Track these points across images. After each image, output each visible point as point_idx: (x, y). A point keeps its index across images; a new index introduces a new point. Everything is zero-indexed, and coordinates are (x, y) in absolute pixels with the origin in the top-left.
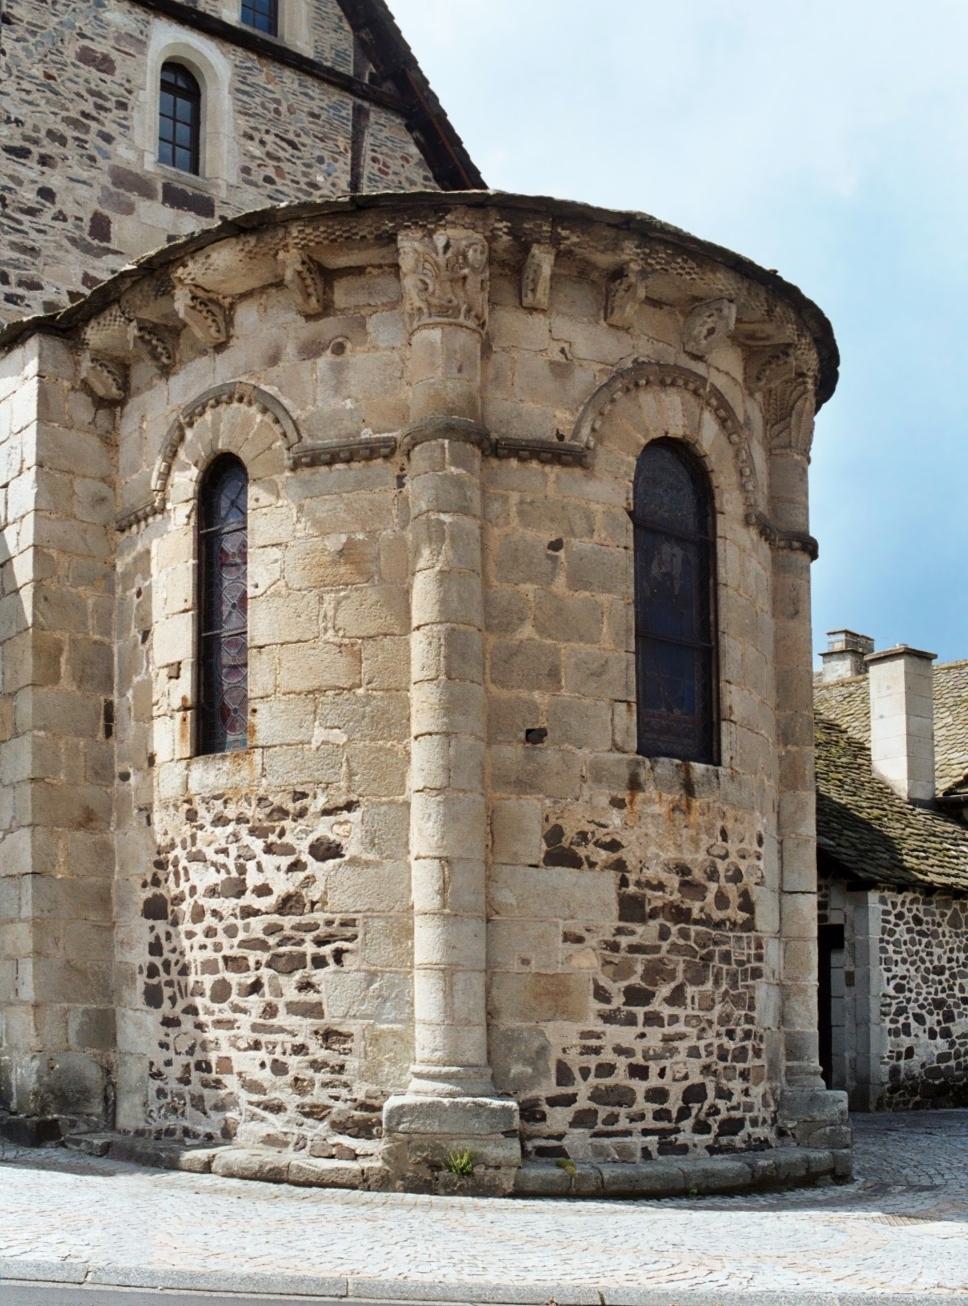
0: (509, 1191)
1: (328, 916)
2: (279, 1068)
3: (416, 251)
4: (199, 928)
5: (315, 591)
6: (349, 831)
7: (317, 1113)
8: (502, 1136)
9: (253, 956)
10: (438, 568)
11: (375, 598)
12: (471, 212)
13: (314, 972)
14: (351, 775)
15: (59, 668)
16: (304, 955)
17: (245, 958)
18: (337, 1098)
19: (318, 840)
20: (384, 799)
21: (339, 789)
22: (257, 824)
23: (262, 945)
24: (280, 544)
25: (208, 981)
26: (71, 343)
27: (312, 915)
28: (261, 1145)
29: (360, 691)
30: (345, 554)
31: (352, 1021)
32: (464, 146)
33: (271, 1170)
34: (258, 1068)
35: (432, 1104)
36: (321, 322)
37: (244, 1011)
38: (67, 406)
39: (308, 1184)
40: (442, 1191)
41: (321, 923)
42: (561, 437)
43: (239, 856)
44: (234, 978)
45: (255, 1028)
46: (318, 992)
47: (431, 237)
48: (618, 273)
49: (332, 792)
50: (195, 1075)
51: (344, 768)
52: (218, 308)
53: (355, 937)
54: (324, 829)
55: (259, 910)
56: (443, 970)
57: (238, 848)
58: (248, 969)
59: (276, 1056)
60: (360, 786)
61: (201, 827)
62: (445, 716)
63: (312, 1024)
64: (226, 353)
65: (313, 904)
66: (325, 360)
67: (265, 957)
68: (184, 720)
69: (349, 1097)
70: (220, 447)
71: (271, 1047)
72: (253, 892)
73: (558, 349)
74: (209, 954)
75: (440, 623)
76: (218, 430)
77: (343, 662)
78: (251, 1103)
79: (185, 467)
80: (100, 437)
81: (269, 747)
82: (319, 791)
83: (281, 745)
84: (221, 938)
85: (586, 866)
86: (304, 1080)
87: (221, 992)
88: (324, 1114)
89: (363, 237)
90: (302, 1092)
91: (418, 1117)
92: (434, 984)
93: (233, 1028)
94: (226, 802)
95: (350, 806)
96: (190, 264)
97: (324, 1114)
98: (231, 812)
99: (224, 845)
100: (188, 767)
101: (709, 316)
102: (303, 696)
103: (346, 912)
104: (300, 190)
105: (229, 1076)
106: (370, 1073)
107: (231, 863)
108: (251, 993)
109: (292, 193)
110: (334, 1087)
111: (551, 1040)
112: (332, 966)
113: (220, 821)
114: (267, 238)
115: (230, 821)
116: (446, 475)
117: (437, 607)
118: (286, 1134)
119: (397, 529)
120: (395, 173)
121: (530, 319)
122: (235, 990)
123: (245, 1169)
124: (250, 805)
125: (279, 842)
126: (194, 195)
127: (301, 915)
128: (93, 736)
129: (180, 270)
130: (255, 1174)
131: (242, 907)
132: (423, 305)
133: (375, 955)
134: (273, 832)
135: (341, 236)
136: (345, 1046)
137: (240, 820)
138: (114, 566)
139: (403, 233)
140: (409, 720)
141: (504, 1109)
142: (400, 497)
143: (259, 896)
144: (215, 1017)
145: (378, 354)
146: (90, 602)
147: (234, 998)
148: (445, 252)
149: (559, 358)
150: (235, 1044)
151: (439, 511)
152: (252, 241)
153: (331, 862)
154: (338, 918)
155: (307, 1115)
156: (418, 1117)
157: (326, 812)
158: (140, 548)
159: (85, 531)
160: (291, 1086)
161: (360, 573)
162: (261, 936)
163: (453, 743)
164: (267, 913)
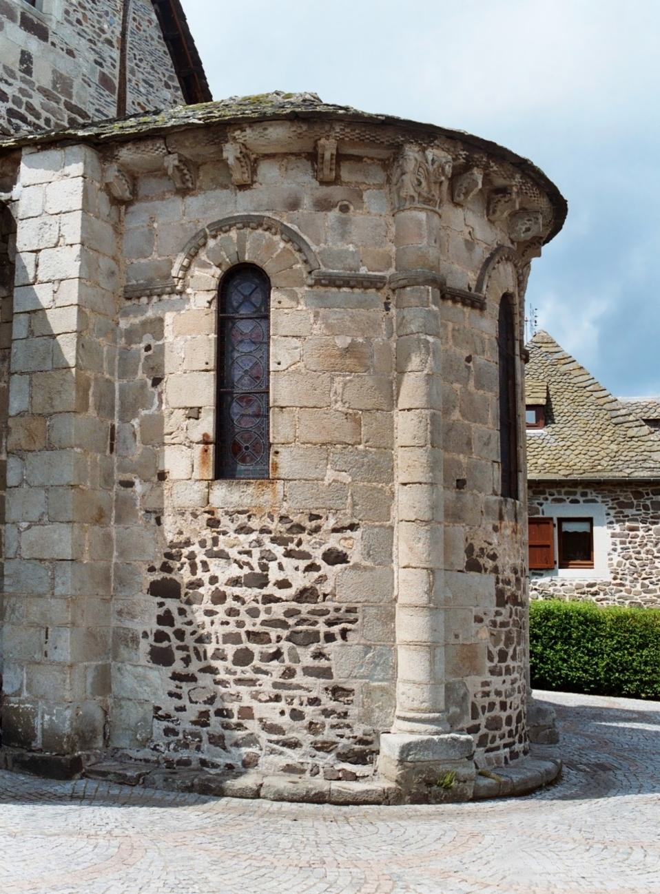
0: (471, 797)
1: (336, 604)
2: (297, 715)
3: (416, 159)
4: (220, 608)
5: (328, 374)
6: (353, 544)
7: (327, 748)
8: (466, 760)
9: (274, 633)
10: (425, 372)
11: (371, 383)
12: (449, 140)
13: (326, 645)
14: (354, 505)
15: (88, 399)
16: (318, 632)
17: (267, 634)
18: (342, 736)
19: (329, 550)
20: (377, 523)
21: (345, 514)
22: (278, 535)
23: (284, 625)
24: (300, 337)
25: (230, 650)
26: (101, 155)
27: (323, 603)
28: (282, 772)
29: (361, 447)
30: (349, 351)
31: (354, 680)
32: (187, 21)
33: (315, 794)
34: (279, 715)
35: (428, 741)
36: (332, 187)
37: (266, 673)
38: (97, 201)
39: (346, 803)
40: (433, 801)
41: (331, 609)
42: (470, 289)
43: (263, 558)
44: (256, 648)
45: (275, 685)
46: (328, 659)
47: (424, 152)
48: (504, 191)
49: (340, 516)
50: (214, 720)
51: (349, 500)
52: (252, 161)
53: (356, 620)
54: (334, 542)
55: (280, 599)
56: (429, 646)
57: (261, 552)
58: (270, 641)
59: (294, 706)
60: (360, 513)
61: (225, 533)
62: (431, 471)
63: (324, 683)
64: (248, 192)
65: (325, 595)
66: (335, 214)
67: (285, 633)
68: (206, 451)
69: (351, 735)
70: (247, 259)
71: (289, 700)
72: (275, 585)
73: (468, 231)
74: (232, 628)
75: (428, 409)
76: (244, 246)
77: (349, 425)
78: (270, 741)
79: (204, 265)
80: (112, 225)
81: (290, 480)
82: (330, 515)
83: (299, 480)
84: (243, 616)
85: (483, 571)
86: (317, 724)
87: (243, 658)
88: (331, 748)
89: (382, 143)
90: (315, 733)
91: (420, 750)
92: (423, 656)
93: (255, 685)
94: (249, 517)
95: (352, 527)
96: (248, 131)
97: (331, 748)
98: (255, 524)
99: (247, 548)
100: (209, 487)
101: (529, 220)
102: (318, 446)
103: (350, 602)
104: (95, 32)
105: (250, 721)
106: (366, 717)
107: (254, 561)
108: (271, 660)
109: (90, 33)
110: (340, 728)
111: (469, 689)
112: (339, 641)
113: (242, 530)
114: (317, 128)
115: (253, 531)
116: (430, 311)
117: (425, 398)
118: (302, 763)
119: (385, 338)
120: (144, 31)
121: (455, 209)
122: (257, 656)
123: (294, 794)
124: (273, 520)
125: (297, 549)
126: (38, 24)
127: (315, 603)
128: (105, 452)
129: (238, 132)
130: (303, 798)
131: (263, 596)
132: (416, 195)
133: (370, 633)
134: (292, 542)
135: (368, 139)
136: (348, 698)
137: (264, 531)
138: (118, 324)
139: (408, 146)
140: (392, 470)
141: (468, 741)
142: (387, 316)
143: (280, 588)
144: (237, 677)
145: (370, 218)
146: (105, 349)
147: (256, 662)
148: (432, 165)
149: (468, 237)
150: (256, 699)
151: (426, 334)
152: (305, 127)
153: (339, 567)
154: (344, 607)
155: (318, 749)
156: (420, 750)
157: (335, 530)
158: (150, 314)
159: (104, 295)
160: (306, 728)
161: (362, 365)
162: (282, 617)
163: (435, 491)
164: (287, 601)
